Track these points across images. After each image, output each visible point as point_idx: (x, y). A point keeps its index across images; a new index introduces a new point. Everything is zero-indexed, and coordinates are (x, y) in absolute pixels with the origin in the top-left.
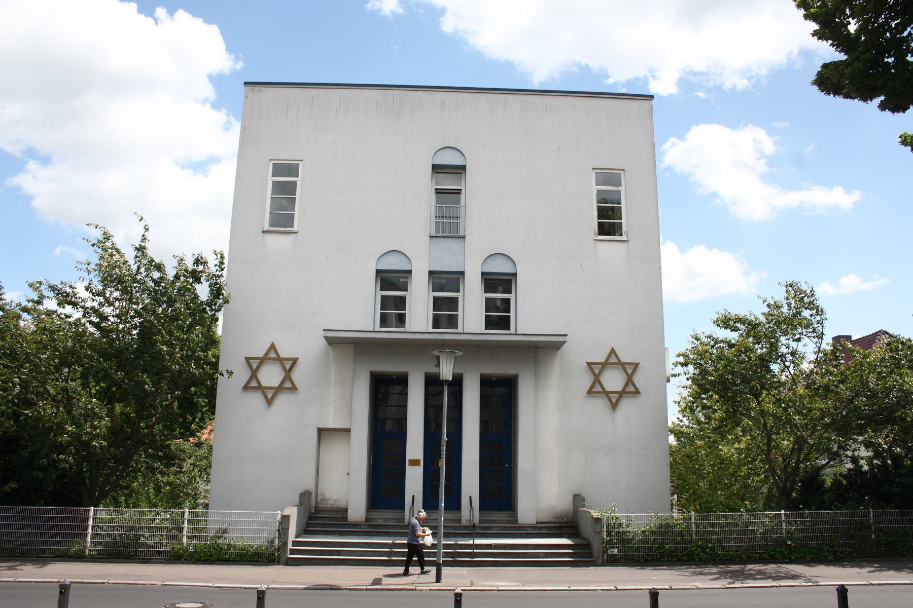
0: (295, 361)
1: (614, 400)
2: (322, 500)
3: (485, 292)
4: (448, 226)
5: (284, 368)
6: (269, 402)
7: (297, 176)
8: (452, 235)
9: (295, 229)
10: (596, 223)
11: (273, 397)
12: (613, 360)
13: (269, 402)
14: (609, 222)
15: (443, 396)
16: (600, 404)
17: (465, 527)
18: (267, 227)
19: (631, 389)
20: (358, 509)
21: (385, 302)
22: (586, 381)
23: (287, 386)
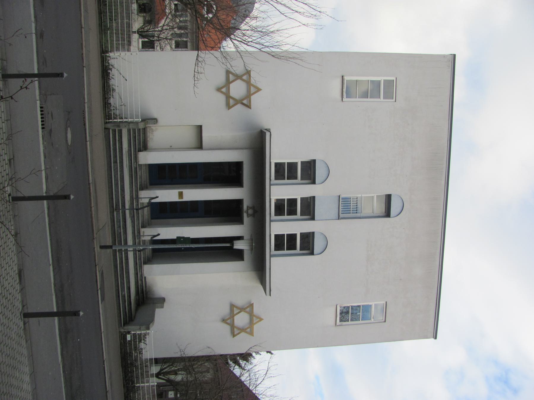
0: (249, 106)
1: (228, 320)
2: (152, 130)
3: (302, 162)
4: (347, 209)
5: (243, 99)
6: (219, 90)
7: (384, 98)
8: (340, 210)
9: (345, 99)
10: (348, 305)
11: (222, 92)
12: (255, 320)
13: (232, 306)
14: (347, 314)
15: (229, 212)
16: (225, 311)
17: (139, 232)
18: (346, 78)
19: (236, 331)
20: (149, 158)
21: (292, 166)
22: (240, 302)
23: (230, 102)
